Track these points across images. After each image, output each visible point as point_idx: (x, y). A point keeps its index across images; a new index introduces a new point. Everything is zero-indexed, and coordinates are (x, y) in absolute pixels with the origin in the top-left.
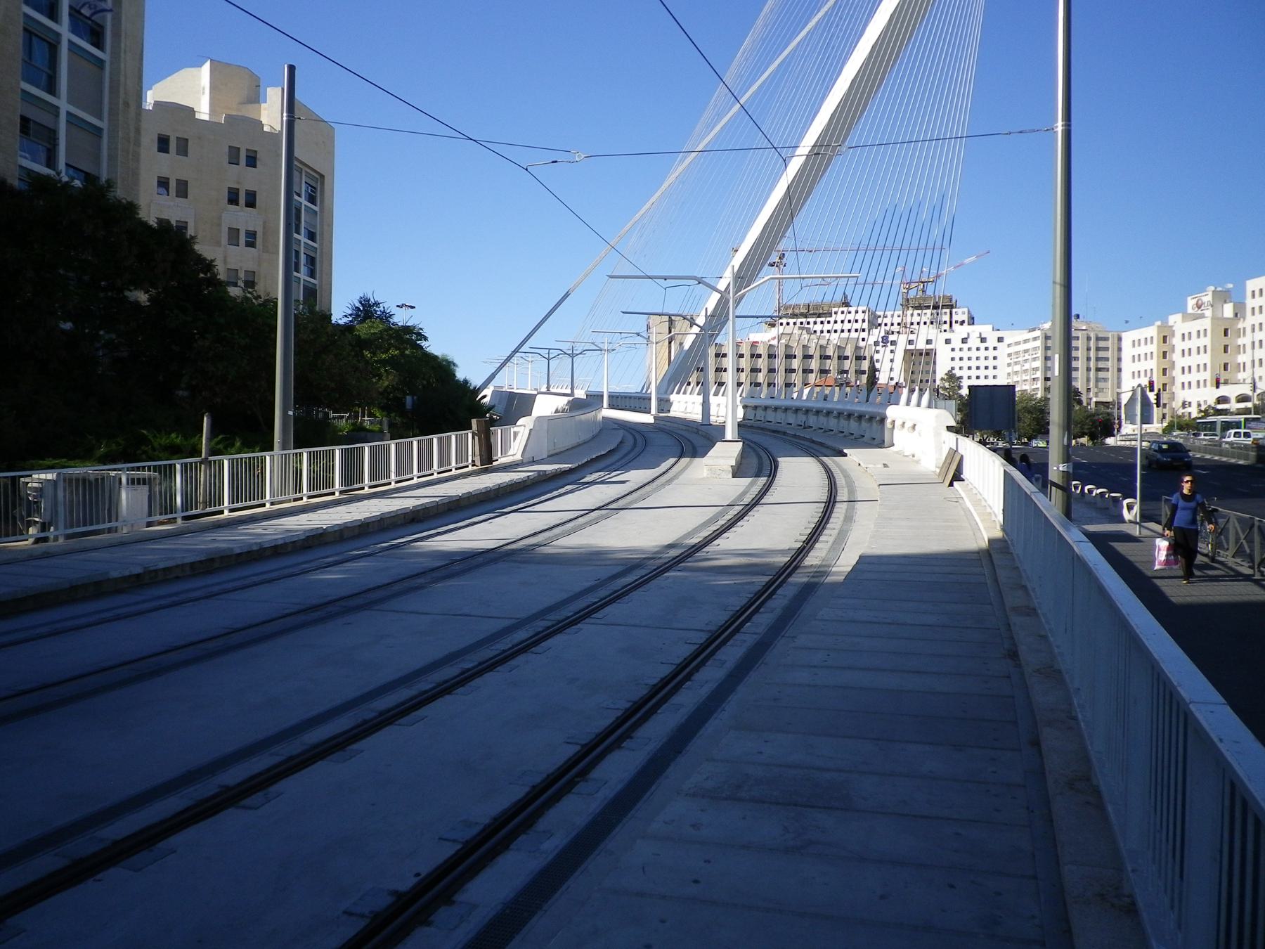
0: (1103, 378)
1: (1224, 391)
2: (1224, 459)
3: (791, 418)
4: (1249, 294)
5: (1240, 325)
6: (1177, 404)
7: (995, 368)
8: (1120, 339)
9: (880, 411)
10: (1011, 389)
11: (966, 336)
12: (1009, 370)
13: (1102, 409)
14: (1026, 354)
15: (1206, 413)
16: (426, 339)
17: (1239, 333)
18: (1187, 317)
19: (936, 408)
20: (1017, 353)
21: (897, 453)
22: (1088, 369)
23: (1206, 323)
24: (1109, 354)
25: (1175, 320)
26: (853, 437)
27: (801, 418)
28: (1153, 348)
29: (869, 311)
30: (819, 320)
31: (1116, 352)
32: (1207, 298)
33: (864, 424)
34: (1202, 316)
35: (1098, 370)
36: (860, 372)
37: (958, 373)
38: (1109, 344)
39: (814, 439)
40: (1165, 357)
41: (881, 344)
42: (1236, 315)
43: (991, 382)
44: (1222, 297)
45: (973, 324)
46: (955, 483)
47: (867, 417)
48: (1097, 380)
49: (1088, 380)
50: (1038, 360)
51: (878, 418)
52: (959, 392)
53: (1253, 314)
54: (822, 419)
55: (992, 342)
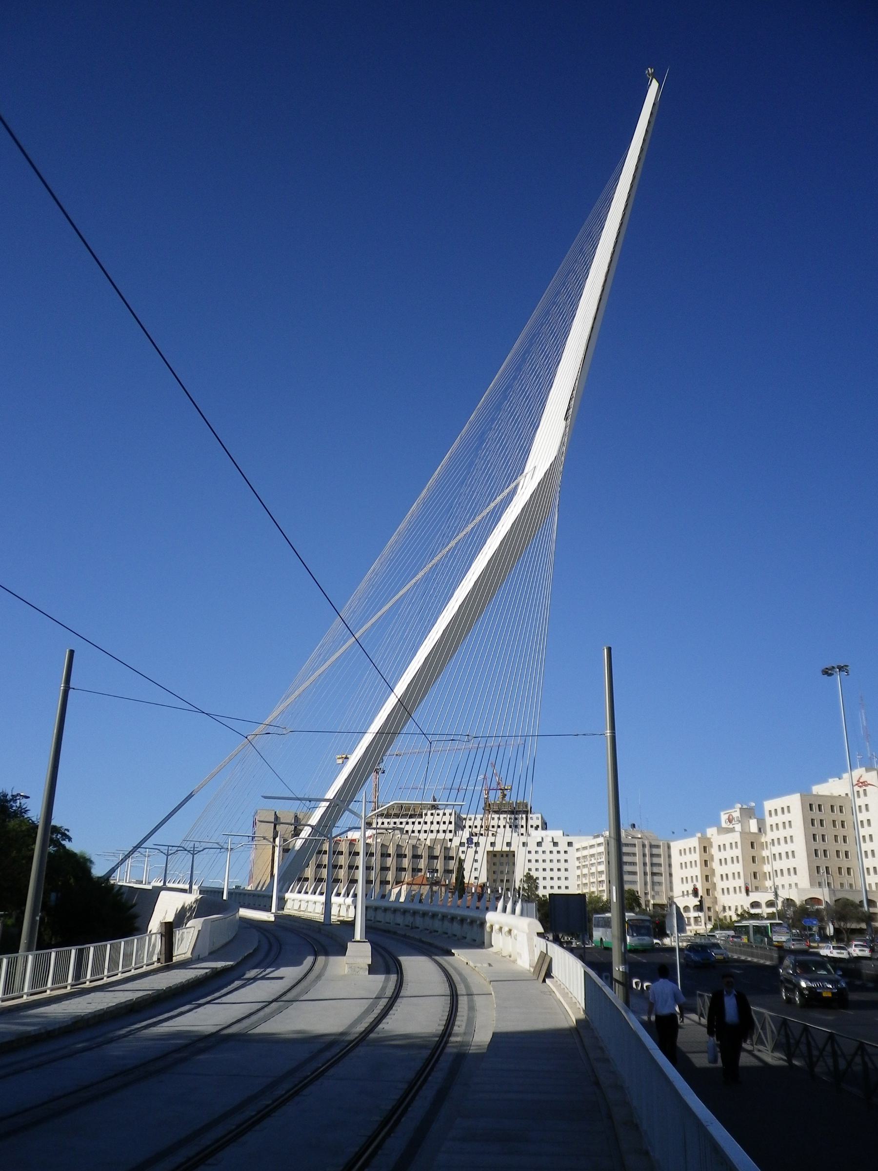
0: (658, 883)
1: (754, 897)
2: (755, 960)
3: (399, 919)
4: (767, 814)
5: (763, 840)
6: (718, 908)
7: (566, 861)
8: (669, 847)
9: (481, 916)
10: (582, 896)
11: (541, 841)
12: (578, 872)
13: (659, 910)
14: (592, 859)
15: (742, 917)
16: (70, 839)
17: (763, 846)
18: (722, 831)
19: (527, 916)
20: (585, 857)
21: (496, 953)
22: (645, 874)
23: (736, 837)
24: (662, 860)
25: (711, 832)
26: (456, 938)
27: (409, 919)
28: (696, 857)
29: (455, 814)
30: (411, 820)
31: (667, 859)
32: (736, 814)
33: (465, 926)
34: (732, 830)
35: (653, 874)
36: (448, 872)
37: (534, 874)
38: (661, 851)
39: (424, 939)
42: (760, 830)
43: (563, 891)
44: (748, 813)
45: (546, 829)
46: (547, 980)
47: (468, 921)
48: (653, 883)
49: (646, 884)
50: (603, 845)
51: (478, 922)
52: (537, 893)
53: (772, 830)
54: (428, 921)
55: (562, 846)
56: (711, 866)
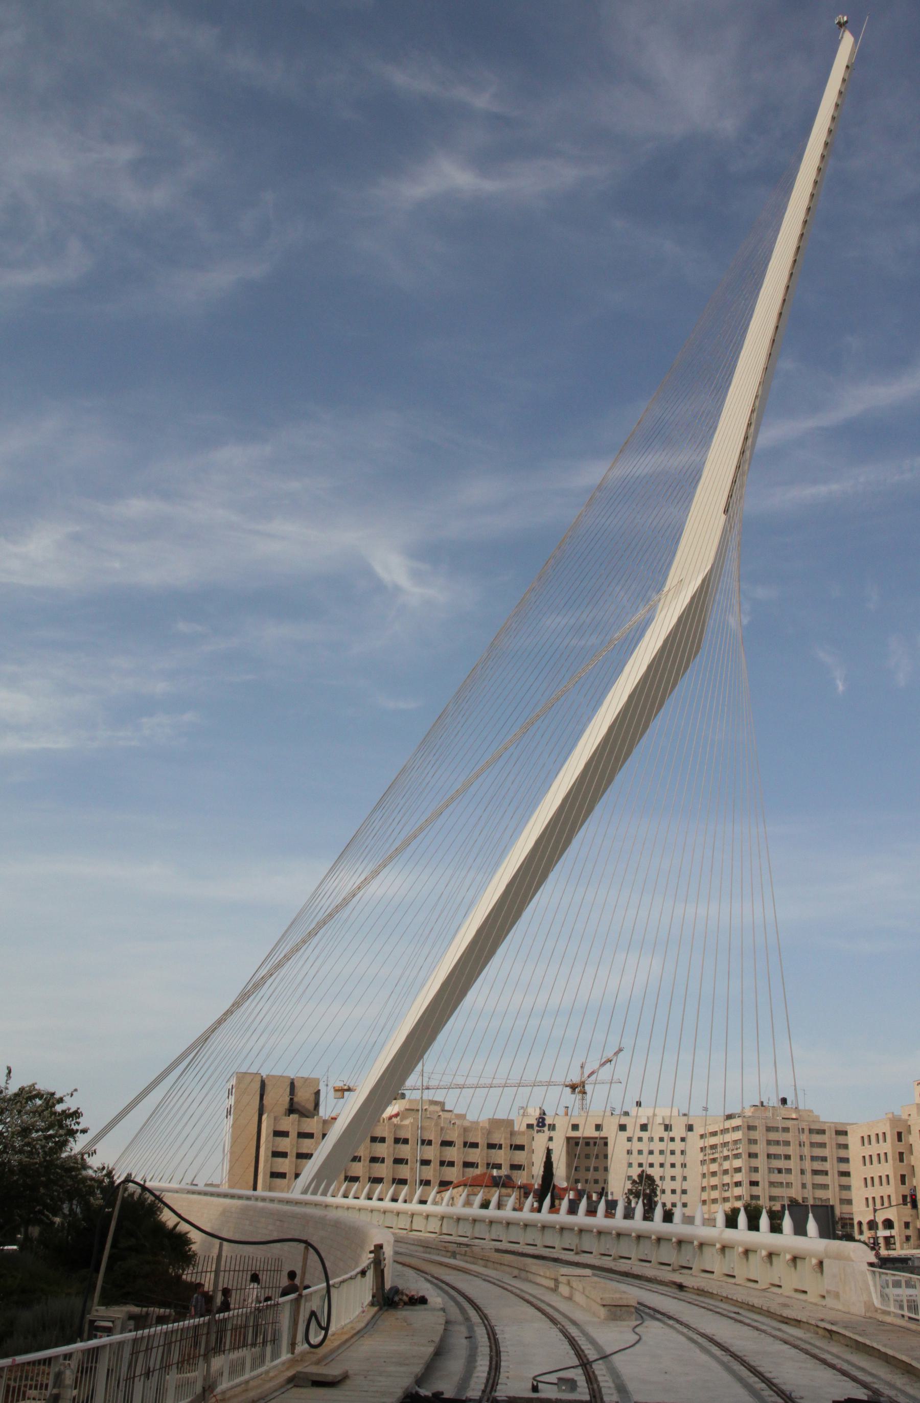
20: (713, 1147)
37: (655, 1172)
40: (901, 1160)
41: (536, 1128)
56: (909, 1160)
